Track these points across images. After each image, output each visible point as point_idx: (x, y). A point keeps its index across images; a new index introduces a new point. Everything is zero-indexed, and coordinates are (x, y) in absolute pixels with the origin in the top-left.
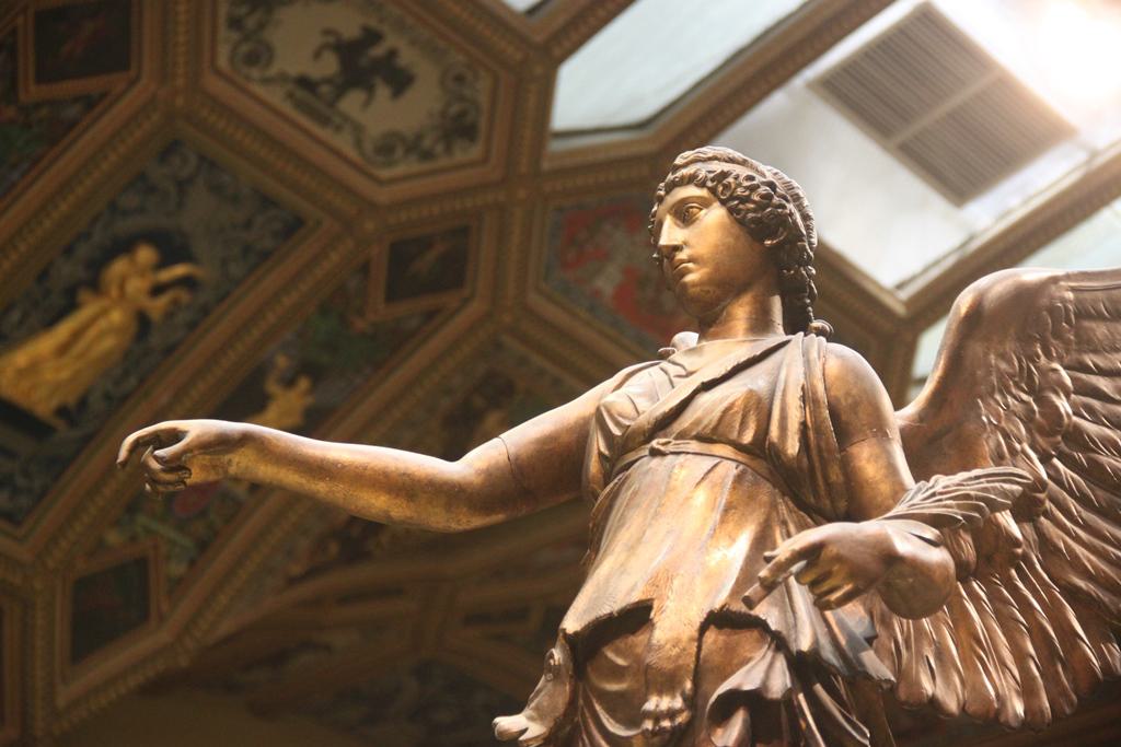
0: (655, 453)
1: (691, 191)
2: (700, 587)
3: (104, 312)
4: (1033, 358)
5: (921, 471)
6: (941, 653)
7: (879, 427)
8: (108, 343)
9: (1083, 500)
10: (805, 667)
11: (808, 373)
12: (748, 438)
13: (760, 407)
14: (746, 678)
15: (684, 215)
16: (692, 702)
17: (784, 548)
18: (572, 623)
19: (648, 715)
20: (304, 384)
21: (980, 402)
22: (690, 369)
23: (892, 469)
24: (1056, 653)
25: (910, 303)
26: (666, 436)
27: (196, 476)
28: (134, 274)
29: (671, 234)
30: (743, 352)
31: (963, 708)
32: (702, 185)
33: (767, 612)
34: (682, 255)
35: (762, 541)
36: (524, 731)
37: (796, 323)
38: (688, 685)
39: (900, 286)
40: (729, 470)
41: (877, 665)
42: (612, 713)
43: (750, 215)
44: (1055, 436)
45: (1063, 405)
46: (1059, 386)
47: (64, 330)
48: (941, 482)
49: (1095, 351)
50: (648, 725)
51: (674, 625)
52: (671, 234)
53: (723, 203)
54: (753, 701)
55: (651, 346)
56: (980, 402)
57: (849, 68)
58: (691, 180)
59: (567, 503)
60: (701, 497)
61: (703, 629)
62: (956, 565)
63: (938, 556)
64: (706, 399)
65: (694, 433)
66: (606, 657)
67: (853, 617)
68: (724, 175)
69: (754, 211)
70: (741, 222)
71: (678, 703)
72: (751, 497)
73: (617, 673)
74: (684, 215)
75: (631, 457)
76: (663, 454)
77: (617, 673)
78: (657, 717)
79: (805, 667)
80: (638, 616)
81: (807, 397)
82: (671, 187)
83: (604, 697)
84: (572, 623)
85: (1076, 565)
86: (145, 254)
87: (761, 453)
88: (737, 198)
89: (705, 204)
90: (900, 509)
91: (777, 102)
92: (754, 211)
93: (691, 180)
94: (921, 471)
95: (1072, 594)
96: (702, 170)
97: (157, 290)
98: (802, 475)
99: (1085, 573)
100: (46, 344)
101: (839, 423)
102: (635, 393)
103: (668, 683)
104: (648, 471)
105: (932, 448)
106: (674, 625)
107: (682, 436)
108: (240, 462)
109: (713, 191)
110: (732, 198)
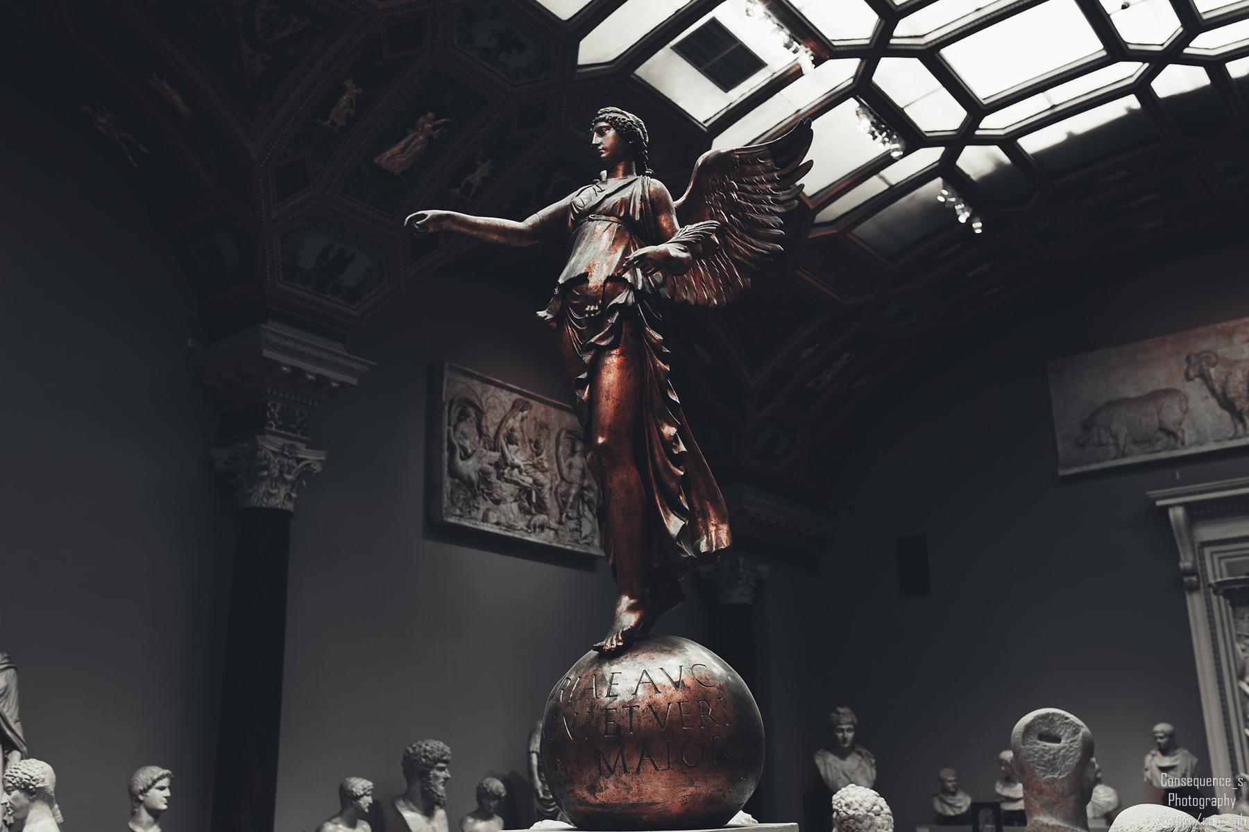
1: (604, 124)
2: (605, 267)
3: (417, 137)
4: (724, 179)
5: (682, 226)
6: (690, 284)
7: (667, 208)
8: (419, 147)
9: (741, 229)
10: (639, 295)
11: (643, 191)
13: (625, 203)
14: (620, 299)
15: (601, 133)
17: (635, 254)
18: (561, 281)
20: (489, 161)
23: (672, 224)
24: (729, 282)
27: (431, 230)
28: (427, 123)
29: (596, 139)
30: (621, 183)
31: (696, 302)
33: (627, 276)
35: (626, 252)
37: (641, 172)
40: (615, 226)
41: (665, 291)
44: (732, 207)
45: (735, 196)
46: (734, 190)
47: (403, 143)
48: (689, 228)
51: (596, 280)
52: (596, 139)
54: (622, 307)
55: (590, 178)
58: (603, 120)
59: (565, 233)
60: (606, 236)
61: (605, 282)
63: (684, 255)
64: (608, 200)
67: (659, 276)
72: (623, 236)
73: (577, 298)
74: (601, 133)
77: (577, 298)
78: (590, 312)
79: (639, 295)
80: (584, 277)
81: (643, 198)
82: (597, 122)
84: (561, 281)
85: (737, 251)
86: (430, 115)
89: (608, 128)
90: (673, 239)
91: (661, 53)
93: (603, 120)
94: (682, 226)
95: (735, 261)
96: (607, 116)
97: (434, 128)
98: (639, 226)
99: (740, 254)
100: (396, 149)
101: (654, 205)
102: (585, 197)
105: (686, 216)
106: (596, 280)
107: (600, 214)
108: (446, 224)
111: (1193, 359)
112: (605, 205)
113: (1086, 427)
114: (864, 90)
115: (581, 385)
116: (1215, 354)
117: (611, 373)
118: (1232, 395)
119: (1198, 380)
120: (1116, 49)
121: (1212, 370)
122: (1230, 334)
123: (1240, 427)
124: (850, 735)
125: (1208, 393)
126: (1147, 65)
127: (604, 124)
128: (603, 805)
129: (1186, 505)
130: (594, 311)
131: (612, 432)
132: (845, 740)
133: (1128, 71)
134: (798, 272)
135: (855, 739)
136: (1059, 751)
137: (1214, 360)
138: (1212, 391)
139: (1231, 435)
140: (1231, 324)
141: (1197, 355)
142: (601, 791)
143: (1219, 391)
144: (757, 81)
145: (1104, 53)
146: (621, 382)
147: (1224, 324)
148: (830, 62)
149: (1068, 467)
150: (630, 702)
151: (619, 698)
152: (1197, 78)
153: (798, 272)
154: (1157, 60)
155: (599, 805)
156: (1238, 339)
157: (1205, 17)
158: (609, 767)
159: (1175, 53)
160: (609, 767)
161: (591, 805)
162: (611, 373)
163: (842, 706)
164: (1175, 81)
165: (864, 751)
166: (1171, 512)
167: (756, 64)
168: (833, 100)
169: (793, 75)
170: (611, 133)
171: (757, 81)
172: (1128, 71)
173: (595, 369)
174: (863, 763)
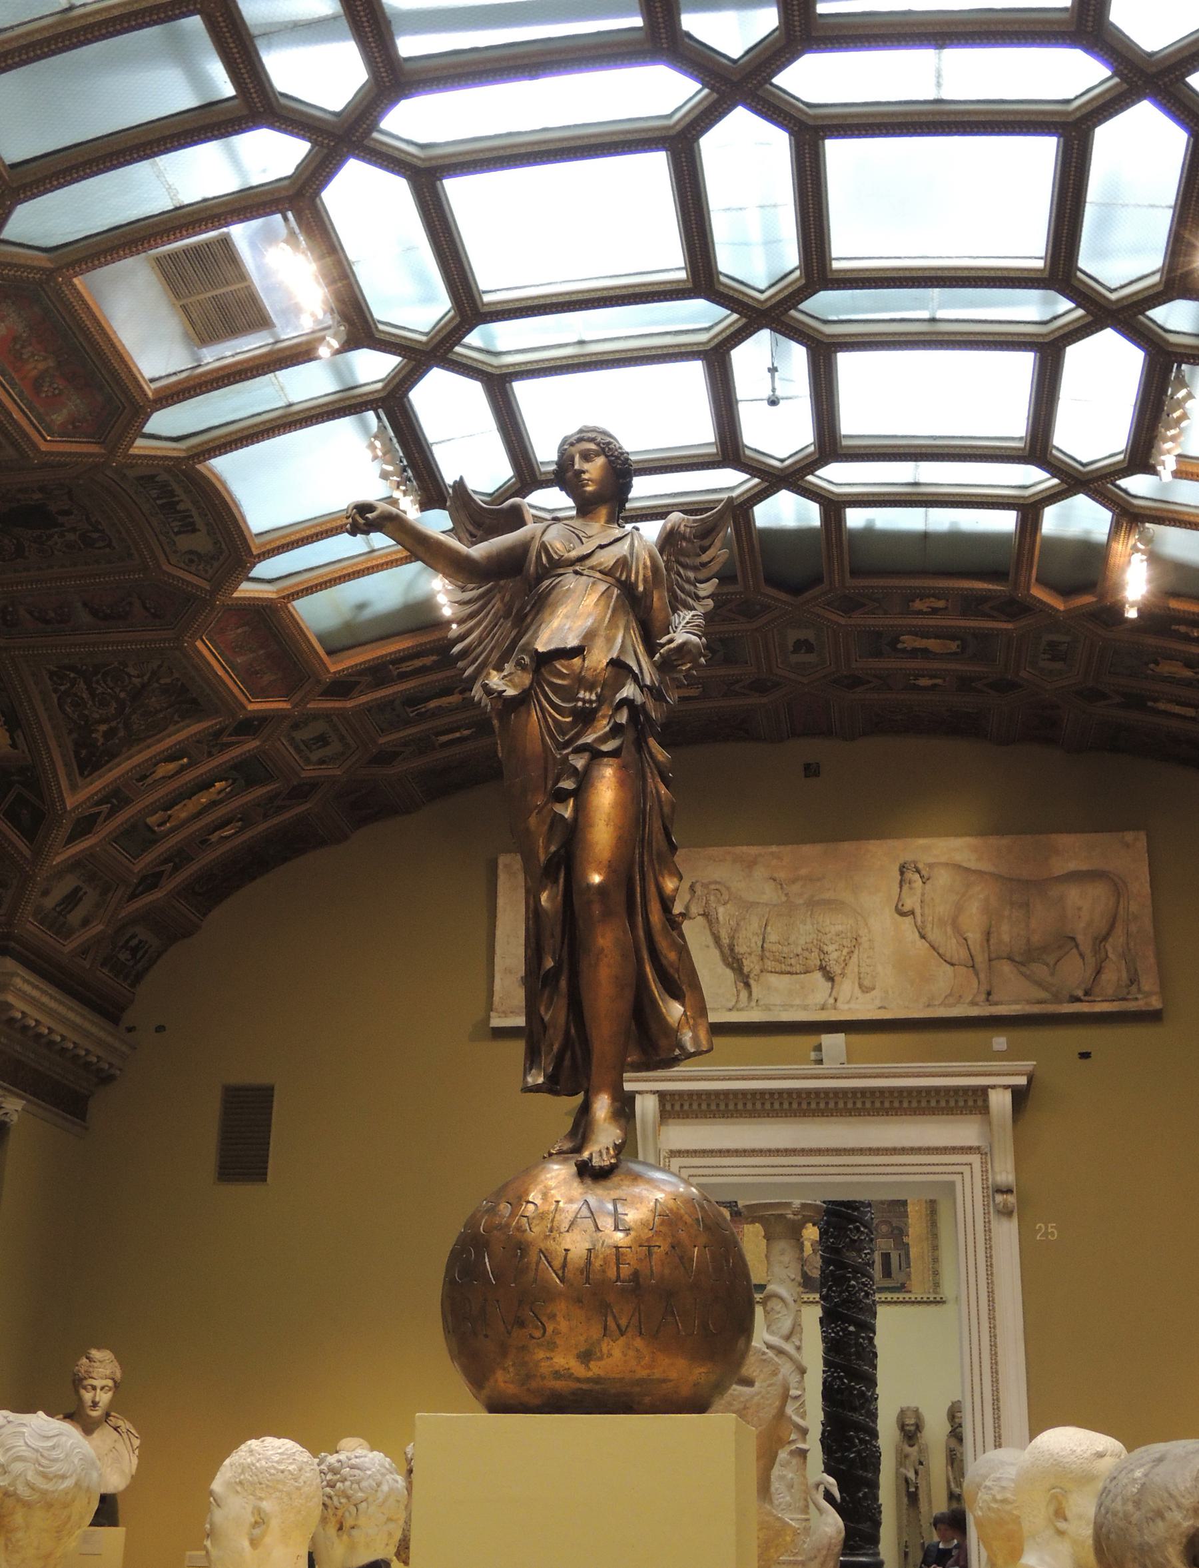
0: (576, 573)
1: (592, 446)
12: (623, 578)
19: (579, 700)
25: (156, 391)
32: (598, 444)
38: (599, 690)
39: (152, 380)
42: (555, 693)
49: (688, 556)
50: (580, 704)
53: (607, 456)
57: (172, 256)
70: (614, 469)
71: (594, 697)
73: (561, 675)
75: (561, 571)
76: (582, 574)
77: (561, 675)
83: (553, 686)
87: (627, 588)
103: (590, 688)
107: (592, 568)
109: (603, 449)
112: (593, 561)
114: (392, 402)
115: (561, 796)
116: (728, 889)
117: (606, 792)
118: (741, 949)
121: (721, 910)
122: (751, 864)
123: (744, 994)
124: (104, 1398)
125: (710, 941)
127: (592, 446)
128: (597, 1380)
129: (662, 1096)
130: (591, 702)
131: (611, 870)
132: (95, 1404)
134: (199, 644)
135: (112, 1404)
136: (752, 1397)
138: (717, 939)
139: (730, 1005)
140: (754, 850)
142: (601, 1359)
143: (725, 941)
144: (250, 345)
146: (619, 804)
149: (505, 1014)
151: (600, 1234)
152: (809, 514)
153: (199, 644)
154: (775, 478)
156: (760, 872)
157: (845, 442)
158: (618, 1326)
159: (791, 477)
160: (618, 1326)
161: (578, 1380)
162: (606, 792)
163: (99, 1348)
164: (785, 512)
165: (124, 1425)
167: (258, 320)
168: (345, 405)
169: (300, 354)
170: (600, 461)
171: (250, 345)
172: (729, 480)
173: (584, 780)
174: (120, 1446)
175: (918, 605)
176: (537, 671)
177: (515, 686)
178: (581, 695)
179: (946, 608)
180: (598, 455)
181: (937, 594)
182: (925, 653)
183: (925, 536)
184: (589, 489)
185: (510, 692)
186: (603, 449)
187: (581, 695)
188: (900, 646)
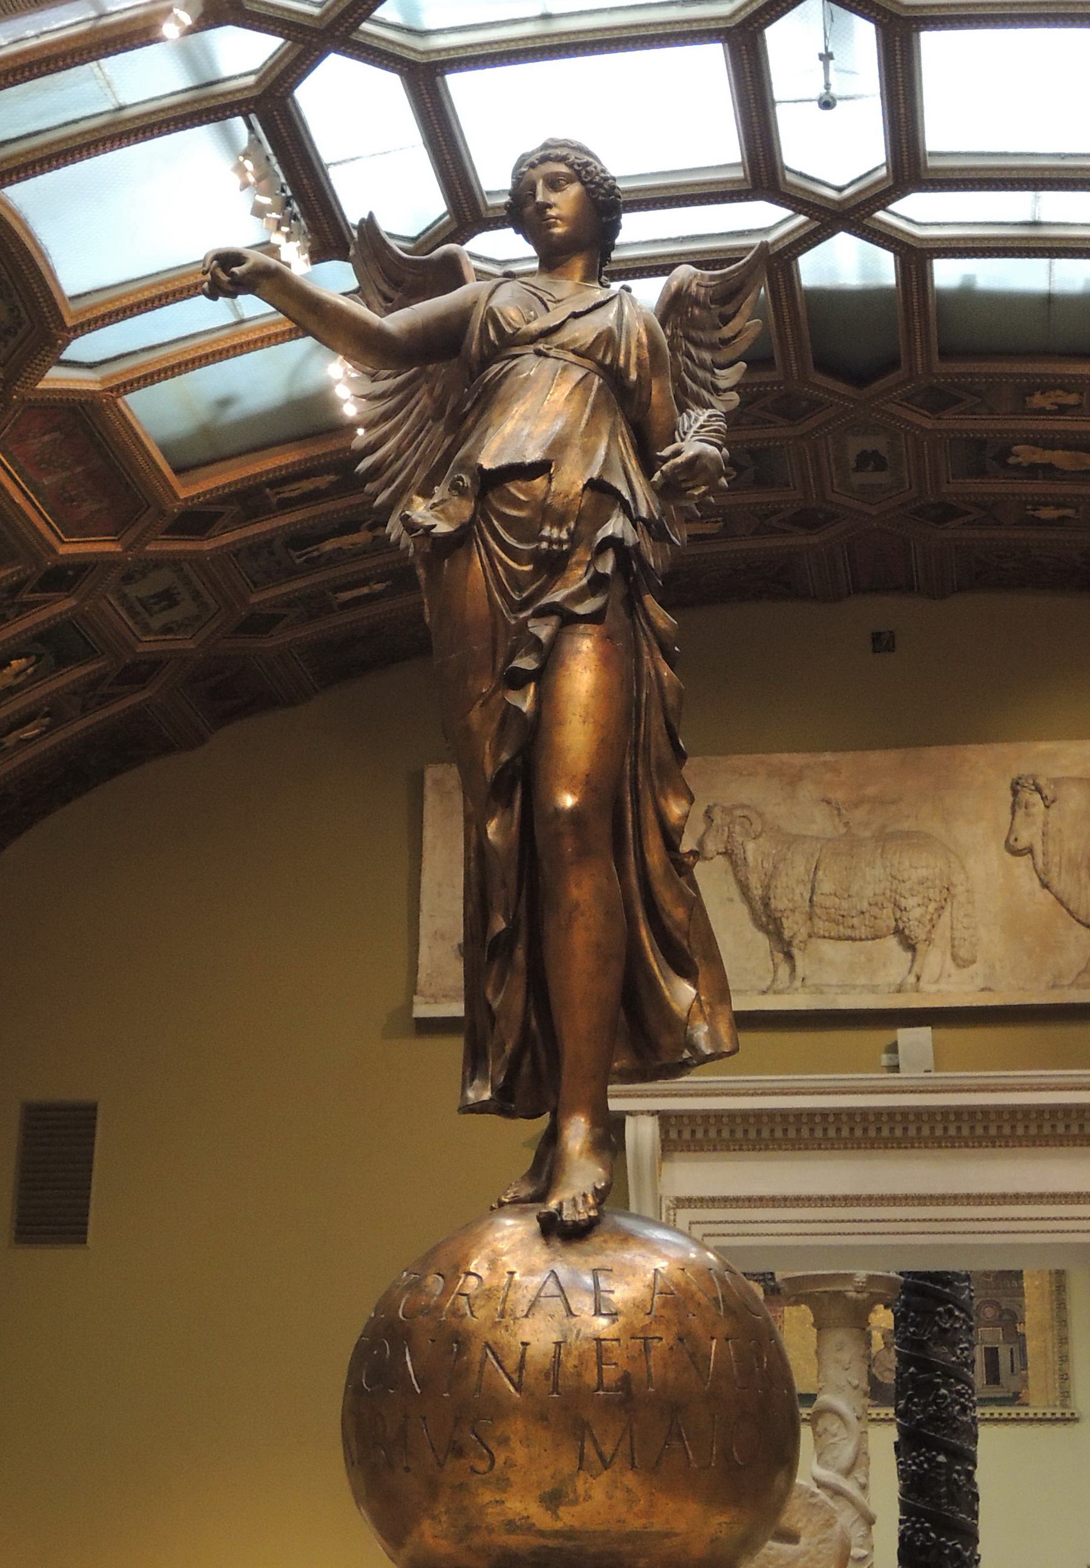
0: (539, 353)
1: (563, 168)
12: (608, 361)
13: (607, 339)
16: (574, 539)
21: (378, 501)
22: (558, 297)
26: (546, 343)
34: (552, 212)
36: (434, 526)
42: (508, 529)
43: (600, 198)
50: (544, 545)
53: (584, 183)
56: (378, 501)
62: (594, 595)
65: (571, 348)
66: (509, 491)
68: (587, 164)
69: (603, 195)
70: (594, 201)
71: (564, 535)
75: (517, 351)
83: (503, 518)
87: (613, 376)
88: (595, 183)
92: (603, 195)
104: (529, 366)
107: (561, 347)
110: (591, 182)
111: (718, 817)
113: (968, 929)
114: (270, 106)
115: (517, 680)
116: (761, 815)
118: (779, 903)
119: (720, 860)
120: (762, 172)
121: (750, 846)
122: (793, 780)
123: (784, 970)
125: (735, 892)
126: (802, 219)
127: (563, 168)
128: (569, 1534)
129: (665, 1118)
130: (560, 542)
131: (590, 787)
133: (762, 218)
136: (796, 1559)
137: (758, 827)
138: (744, 889)
139: (764, 986)
140: (798, 759)
141: (727, 811)
142: (575, 1502)
143: (757, 892)
145: (739, 174)
147: (785, 757)
148: (230, 29)
149: (435, 999)
150: (644, 1328)
152: (880, 268)
155: (556, 1534)
156: (807, 791)
157: (931, 163)
158: (601, 1455)
159: (852, 213)
160: (601, 1455)
161: (541, 1533)
162: (582, 674)
164: (844, 264)
166: (630, 1123)
168: (201, 108)
170: (574, 190)
172: (762, 218)
173: (551, 657)
175: (1038, 400)
176: (481, 497)
177: (449, 519)
178: (546, 532)
179: (1079, 405)
180: (570, 181)
181: (1067, 385)
182: (1049, 470)
183: (1049, 301)
184: (558, 230)
185: (443, 528)
186: (578, 173)
187: (546, 532)
188: (1012, 460)
